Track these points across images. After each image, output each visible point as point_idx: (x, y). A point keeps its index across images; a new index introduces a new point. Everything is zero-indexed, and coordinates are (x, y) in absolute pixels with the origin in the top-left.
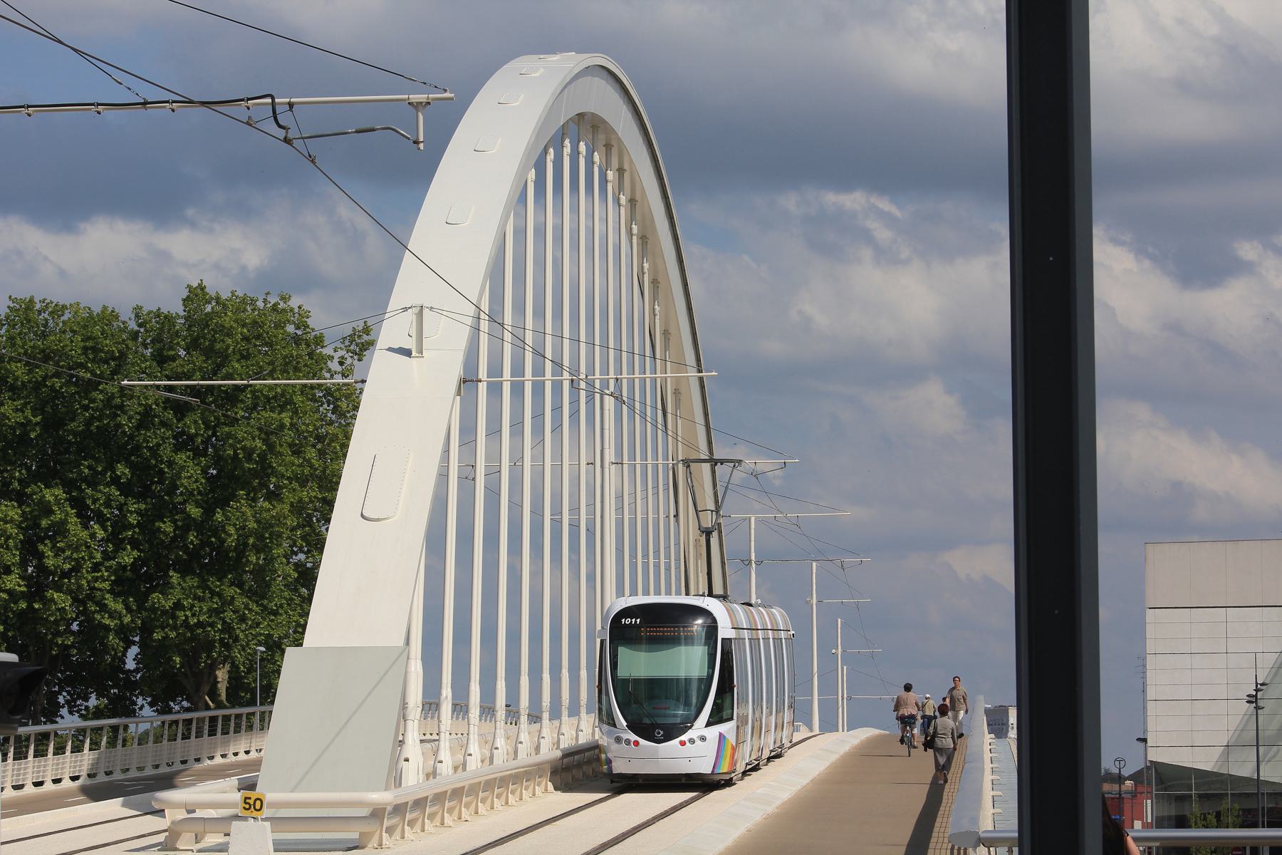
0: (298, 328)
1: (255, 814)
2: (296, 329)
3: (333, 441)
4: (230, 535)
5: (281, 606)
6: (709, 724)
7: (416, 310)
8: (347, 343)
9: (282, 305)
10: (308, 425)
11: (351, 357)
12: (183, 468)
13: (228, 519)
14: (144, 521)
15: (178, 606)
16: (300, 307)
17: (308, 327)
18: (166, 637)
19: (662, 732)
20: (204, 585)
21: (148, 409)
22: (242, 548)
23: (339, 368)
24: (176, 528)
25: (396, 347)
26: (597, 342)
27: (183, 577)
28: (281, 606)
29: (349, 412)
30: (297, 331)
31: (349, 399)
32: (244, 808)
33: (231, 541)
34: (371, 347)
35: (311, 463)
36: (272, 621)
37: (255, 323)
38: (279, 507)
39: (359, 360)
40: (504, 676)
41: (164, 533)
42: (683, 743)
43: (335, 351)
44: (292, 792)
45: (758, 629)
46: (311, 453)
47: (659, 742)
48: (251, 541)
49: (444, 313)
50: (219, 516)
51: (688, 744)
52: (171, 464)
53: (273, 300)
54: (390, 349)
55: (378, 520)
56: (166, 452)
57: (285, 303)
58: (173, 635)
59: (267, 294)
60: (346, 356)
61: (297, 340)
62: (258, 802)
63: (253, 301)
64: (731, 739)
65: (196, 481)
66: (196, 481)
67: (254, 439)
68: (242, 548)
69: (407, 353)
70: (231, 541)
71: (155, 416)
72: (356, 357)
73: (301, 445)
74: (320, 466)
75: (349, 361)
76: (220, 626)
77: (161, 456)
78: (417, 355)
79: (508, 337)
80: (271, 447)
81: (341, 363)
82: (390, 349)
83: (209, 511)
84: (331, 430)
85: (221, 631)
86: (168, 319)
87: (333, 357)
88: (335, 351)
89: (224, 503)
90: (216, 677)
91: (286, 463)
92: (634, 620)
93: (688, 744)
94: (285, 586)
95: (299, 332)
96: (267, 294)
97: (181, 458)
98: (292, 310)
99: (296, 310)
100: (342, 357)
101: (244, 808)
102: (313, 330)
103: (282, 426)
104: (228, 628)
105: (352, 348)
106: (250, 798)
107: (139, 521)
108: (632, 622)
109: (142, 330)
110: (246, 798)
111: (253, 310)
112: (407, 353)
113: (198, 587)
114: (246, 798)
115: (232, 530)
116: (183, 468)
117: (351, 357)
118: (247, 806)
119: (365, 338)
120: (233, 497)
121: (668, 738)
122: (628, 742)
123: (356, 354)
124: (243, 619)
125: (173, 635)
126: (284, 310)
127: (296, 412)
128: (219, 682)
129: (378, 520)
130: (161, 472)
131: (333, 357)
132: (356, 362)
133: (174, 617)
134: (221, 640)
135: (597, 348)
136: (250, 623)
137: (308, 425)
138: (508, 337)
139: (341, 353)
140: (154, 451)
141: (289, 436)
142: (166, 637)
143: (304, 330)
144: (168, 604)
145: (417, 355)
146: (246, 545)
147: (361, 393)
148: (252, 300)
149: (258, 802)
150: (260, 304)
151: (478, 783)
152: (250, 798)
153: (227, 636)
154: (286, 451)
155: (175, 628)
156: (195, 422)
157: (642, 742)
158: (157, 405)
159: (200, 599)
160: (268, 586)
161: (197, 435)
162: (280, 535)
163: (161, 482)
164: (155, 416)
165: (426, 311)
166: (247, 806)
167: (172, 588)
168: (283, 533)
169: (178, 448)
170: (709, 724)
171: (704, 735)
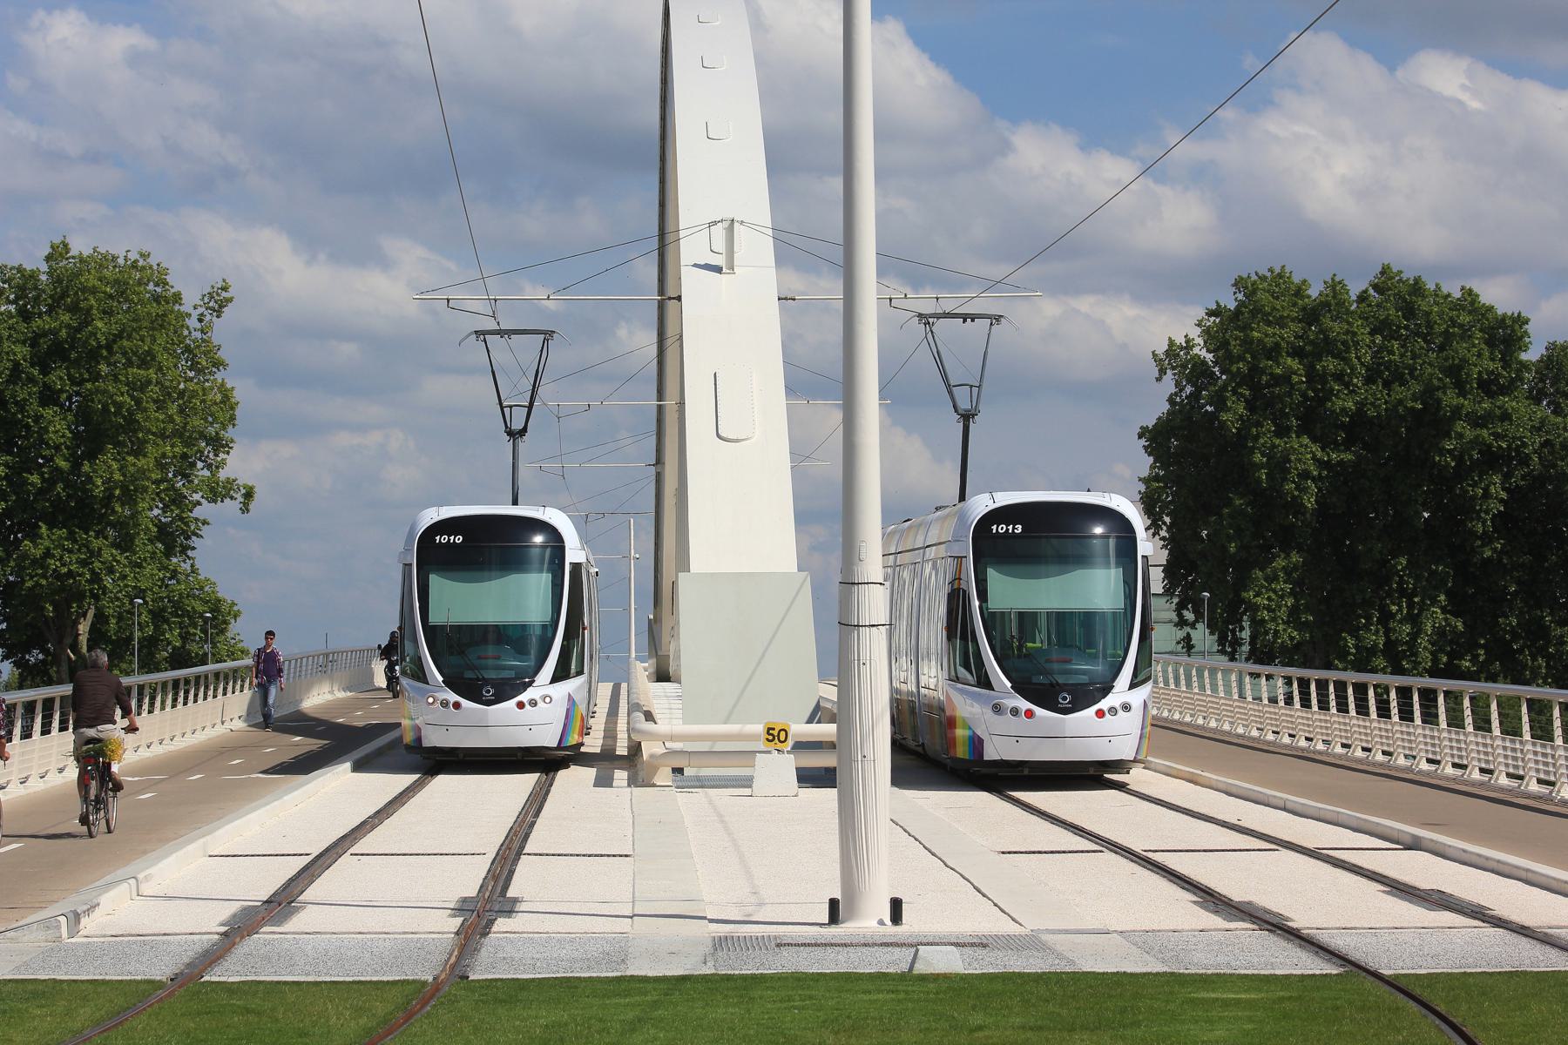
0: (157, 285)
1: (780, 746)
2: (155, 286)
3: (193, 397)
4: (98, 487)
5: (145, 559)
7: (726, 224)
8: (206, 300)
9: (141, 263)
10: (172, 381)
11: (210, 314)
12: (50, 422)
13: (95, 471)
14: (12, 474)
15: (48, 554)
16: (158, 265)
17: (167, 284)
18: (37, 584)
20: (71, 537)
21: (16, 364)
22: (108, 498)
23: (198, 326)
24: (43, 480)
25: (703, 263)
27: (50, 529)
28: (145, 559)
29: (208, 368)
30: (156, 288)
31: (209, 356)
32: (767, 739)
33: (99, 491)
34: (230, 304)
35: (173, 418)
36: (138, 573)
37: (117, 281)
38: (143, 461)
39: (218, 317)
41: (32, 484)
42: (521, 705)
43: (195, 308)
44: (725, 723)
45: (855, 583)
46: (173, 409)
47: (489, 703)
48: (117, 492)
50: (86, 467)
51: (527, 706)
52: (37, 418)
53: (133, 256)
54: (695, 265)
56: (34, 407)
57: (144, 260)
58: (44, 582)
59: (128, 251)
60: (206, 313)
61: (157, 299)
62: (783, 733)
63: (114, 258)
64: (581, 699)
65: (63, 436)
66: (63, 436)
67: (122, 394)
68: (108, 498)
69: (718, 270)
70: (99, 491)
71: (23, 372)
72: (215, 314)
73: (164, 401)
74: (181, 422)
75: (208, 318)
76: (88, 576)
77: (27, 411)
78: (728, 271)
80: (138, 402)
81: (200, 320)
82: (695, 265)
83: (76, 465)
84: (191, 386)
85: (89, 582)
86: (33, 276)
87: (190, 315)
88: (195, 308)
89: (92, 455)
90: (78, 630)
91: (153, 418)
93: (527, 706)
94: (148, 540)
95: (159, 290)
96: (128, 251)
97: (48, 412)
98: (151, 267)
99: (155, 267)
100: (202, 314)
101: (767, 739)
102: (172, 287)
103: (149, 382)
104: (96, 578)
105: (211, 304)
106: (774, 729)
107: (7, 474)
109: (6, 286)
110: (769, 729)
111: (115, 267)
112: (718, 270)
113: (67, 539)
114: (769, 729)
115: (99, 482)
116: (50, 422)
117: (210, 314)
118: (771, 738)
119: (224, 294)
120: (101, 450)
121: (499, 698)
122: (445, 704)
123: (214, 311)
124: (111, 571)
125: (44, 582)
126: (143, 268)
127: (160, 369)
128: (80, 634)
130: (28, 427)
131: (190, 315)
132: (215, 319)
133: (45, 567)
134: (91, 591)
136: (118, 575)
137: (172, 381)
139: (200, 310)
140: (21, 405)
141: (154, 391)
142: (37, 584)
143: (163, 287)
144: (38, 553)
145: (728, 271)
146: (112, 496)
147: (219, 349)
148: (114, 258)
149: (783, 733)
150: (121, 261)
151: (820, 723)
152: (774, 729)
153: (96, 586)
154: (152, 406)
155: (44, 576)
156: (61, 378)
157: (465, 703)
158: (25, 361)
159: (70, 551)
160: (132, 540)
161: (61, 391)
162: (145, 489)
163: (26, 438)
164: (23, 372)
165: (736, 224)
166: (771, 738)
167: (41, 538)
168: (148, 487)
169: (44, 402)
171: (533, 697)
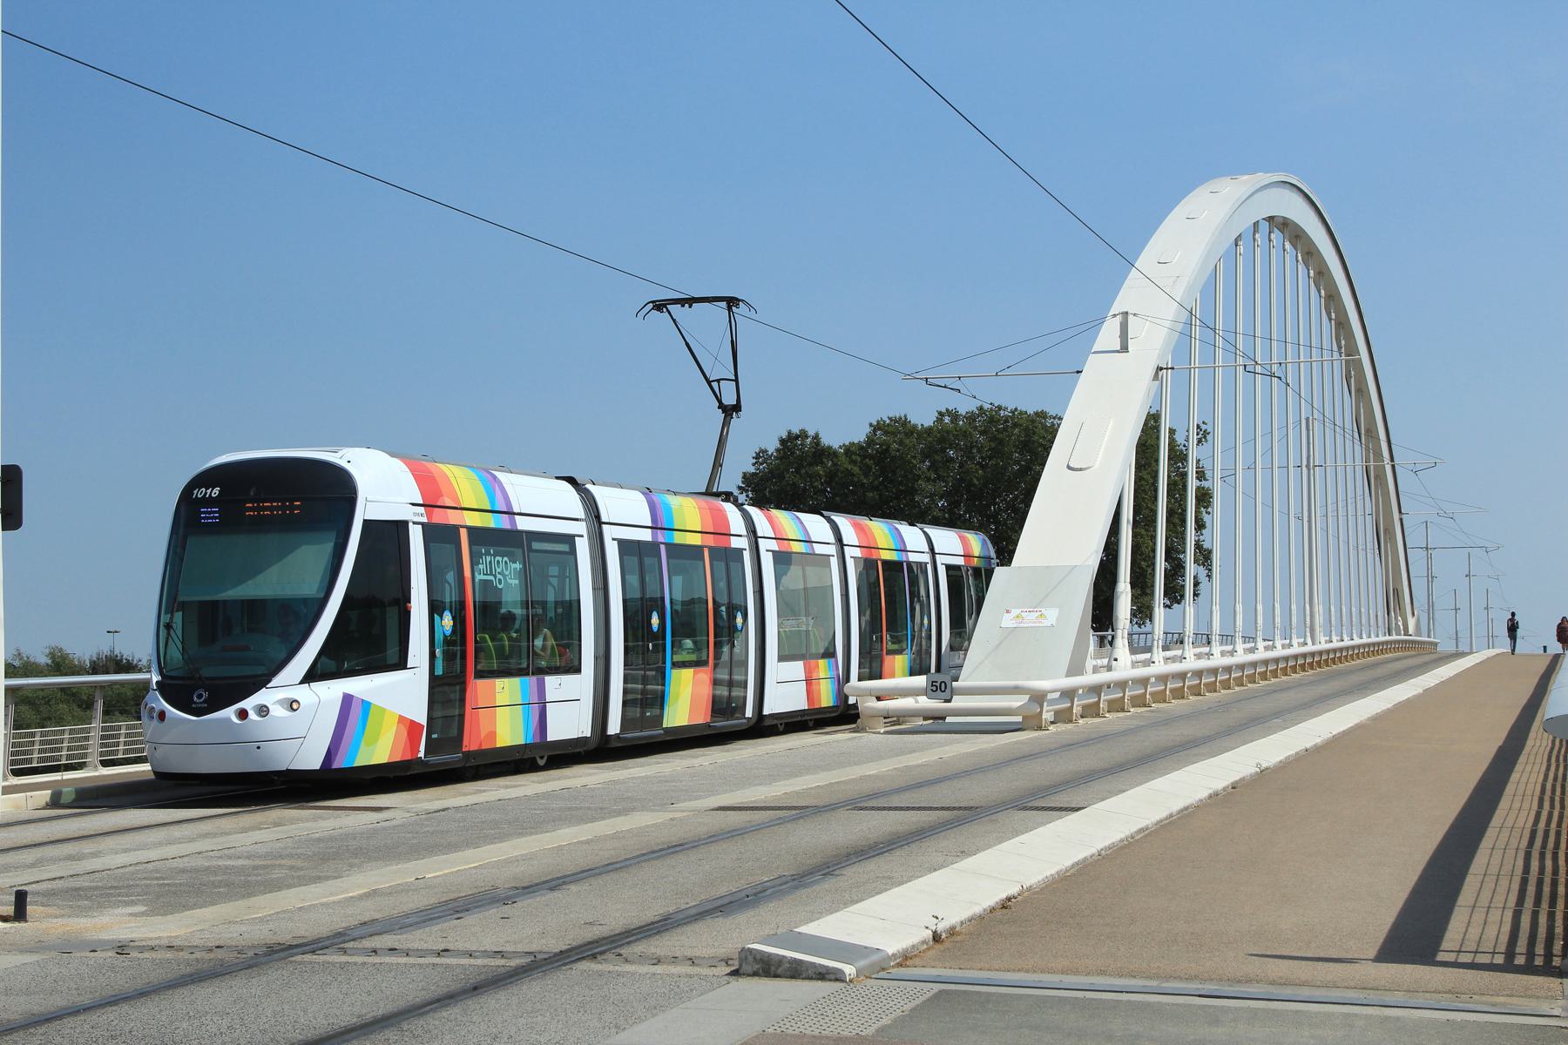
6: (311, 676)
19: (205, 695)
26: (1258, 333)
32: (932, 690)
40: (1128, 580)
47: (198, 712)
49: (1149, 319)
55: (1081, 470)
62: (943, 684)
79: (1220, 342)
92: (209, 491)
101: (932, 690)
108: (206, 493)
118: (934, 688)
129: (1081, 470)
135: (1258, 341)
138: (1220, 342)
149: (943, 684)
165: (1131, 317)
170: (311, 676)
